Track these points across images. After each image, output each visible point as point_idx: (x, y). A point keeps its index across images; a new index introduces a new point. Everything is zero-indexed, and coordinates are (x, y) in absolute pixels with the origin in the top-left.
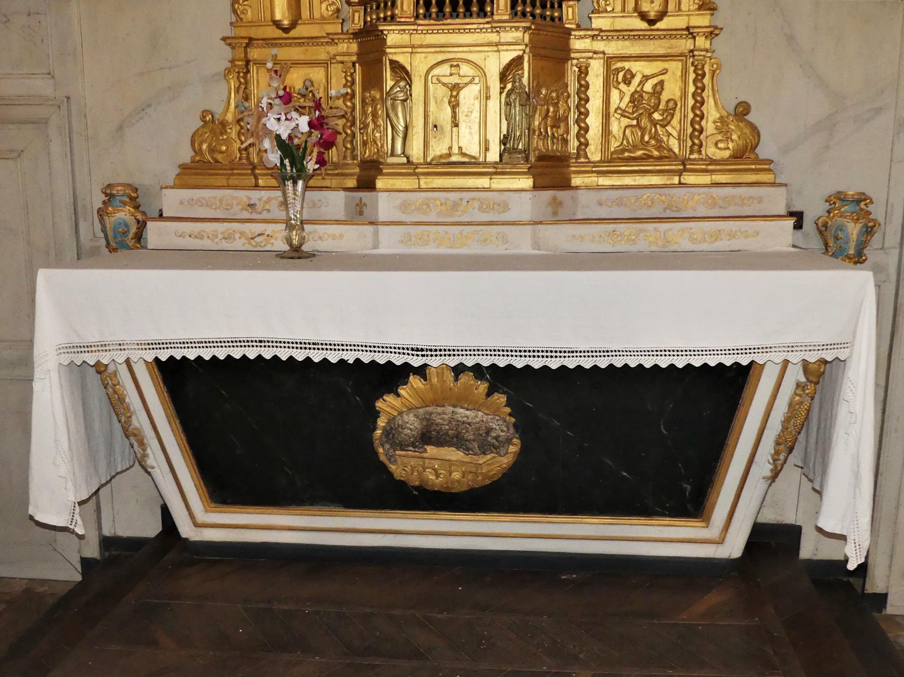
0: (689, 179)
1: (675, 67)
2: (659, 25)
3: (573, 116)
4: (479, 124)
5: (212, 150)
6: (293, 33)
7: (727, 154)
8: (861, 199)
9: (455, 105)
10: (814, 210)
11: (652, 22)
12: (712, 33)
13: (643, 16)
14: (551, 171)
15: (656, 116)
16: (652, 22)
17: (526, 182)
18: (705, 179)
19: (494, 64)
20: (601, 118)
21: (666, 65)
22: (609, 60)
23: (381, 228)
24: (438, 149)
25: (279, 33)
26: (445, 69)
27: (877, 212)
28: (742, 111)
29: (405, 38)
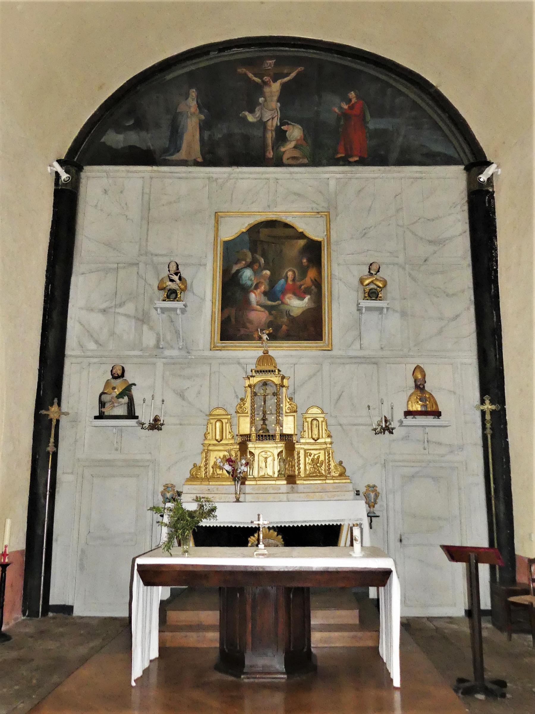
0: (328, 481)
1: (322, 452)
2: (317, 441)
3: (296, 465)
4: (273, 467)
5: (196, 475)
6: (221, 443)
7: (337, 475)
8: (374, 486)
9: (266, 462)
10: (363, 490)
11: (316, 441)
12: (331, 443)
13: (314, 439)
14: (291, 479)
15: (318, 465)
16: (316, 441)
17: (285, 482)
18: (332, 481)
19: (276, 452)
20: (303, 465)
21: (320, 451)
22: (305, 450)
23: (247, 495)
24: (262, 474)
25: (217, 442)
26: (263, 453)
27: (379, 490)
28: (341, 463)
29: (253, 446)
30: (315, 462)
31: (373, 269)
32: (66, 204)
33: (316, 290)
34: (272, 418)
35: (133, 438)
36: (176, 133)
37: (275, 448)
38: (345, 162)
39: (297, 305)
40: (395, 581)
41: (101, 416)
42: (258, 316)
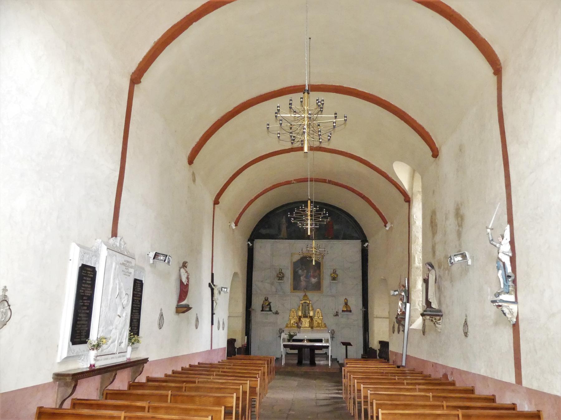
14: (312, 328)
20: (315, 324)
30: (318, 323)
31: (335, 272)
32: (251, 252)
33: (319, 277)
34: (307, 312)
35: (271, 317)
36: (280, 230)
37: (308, 320)
38: (327, 239)
39: (314, 280)
40: (330, 348)
41: (262, 311)
42: (303, 284)
